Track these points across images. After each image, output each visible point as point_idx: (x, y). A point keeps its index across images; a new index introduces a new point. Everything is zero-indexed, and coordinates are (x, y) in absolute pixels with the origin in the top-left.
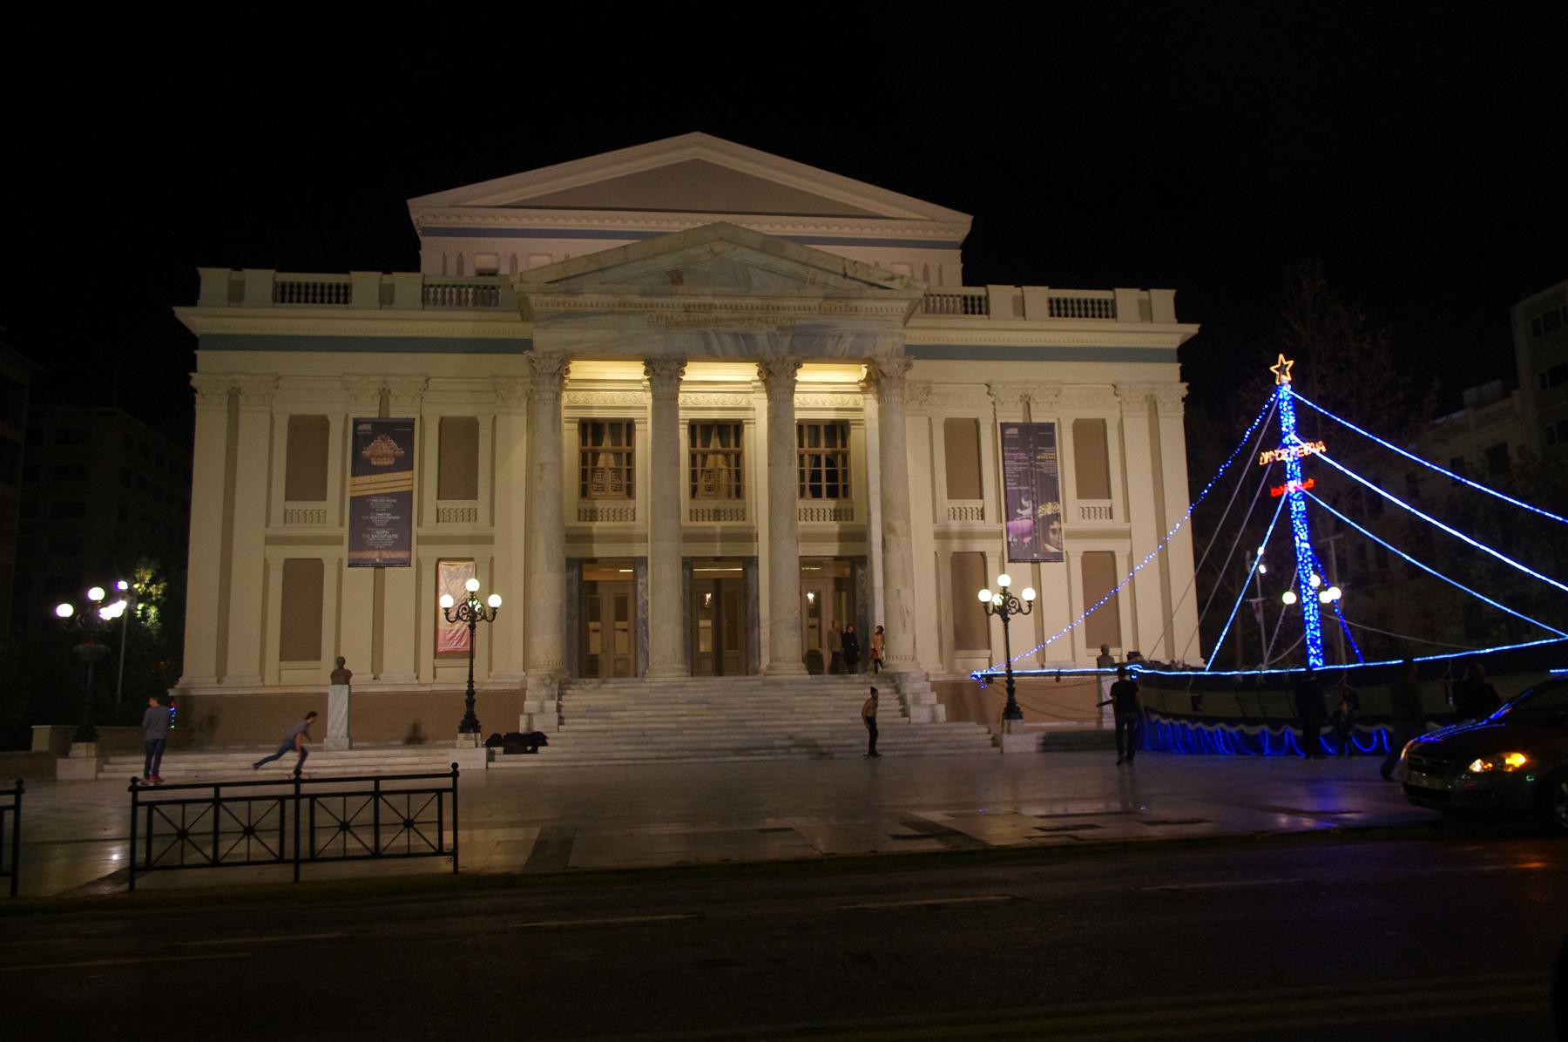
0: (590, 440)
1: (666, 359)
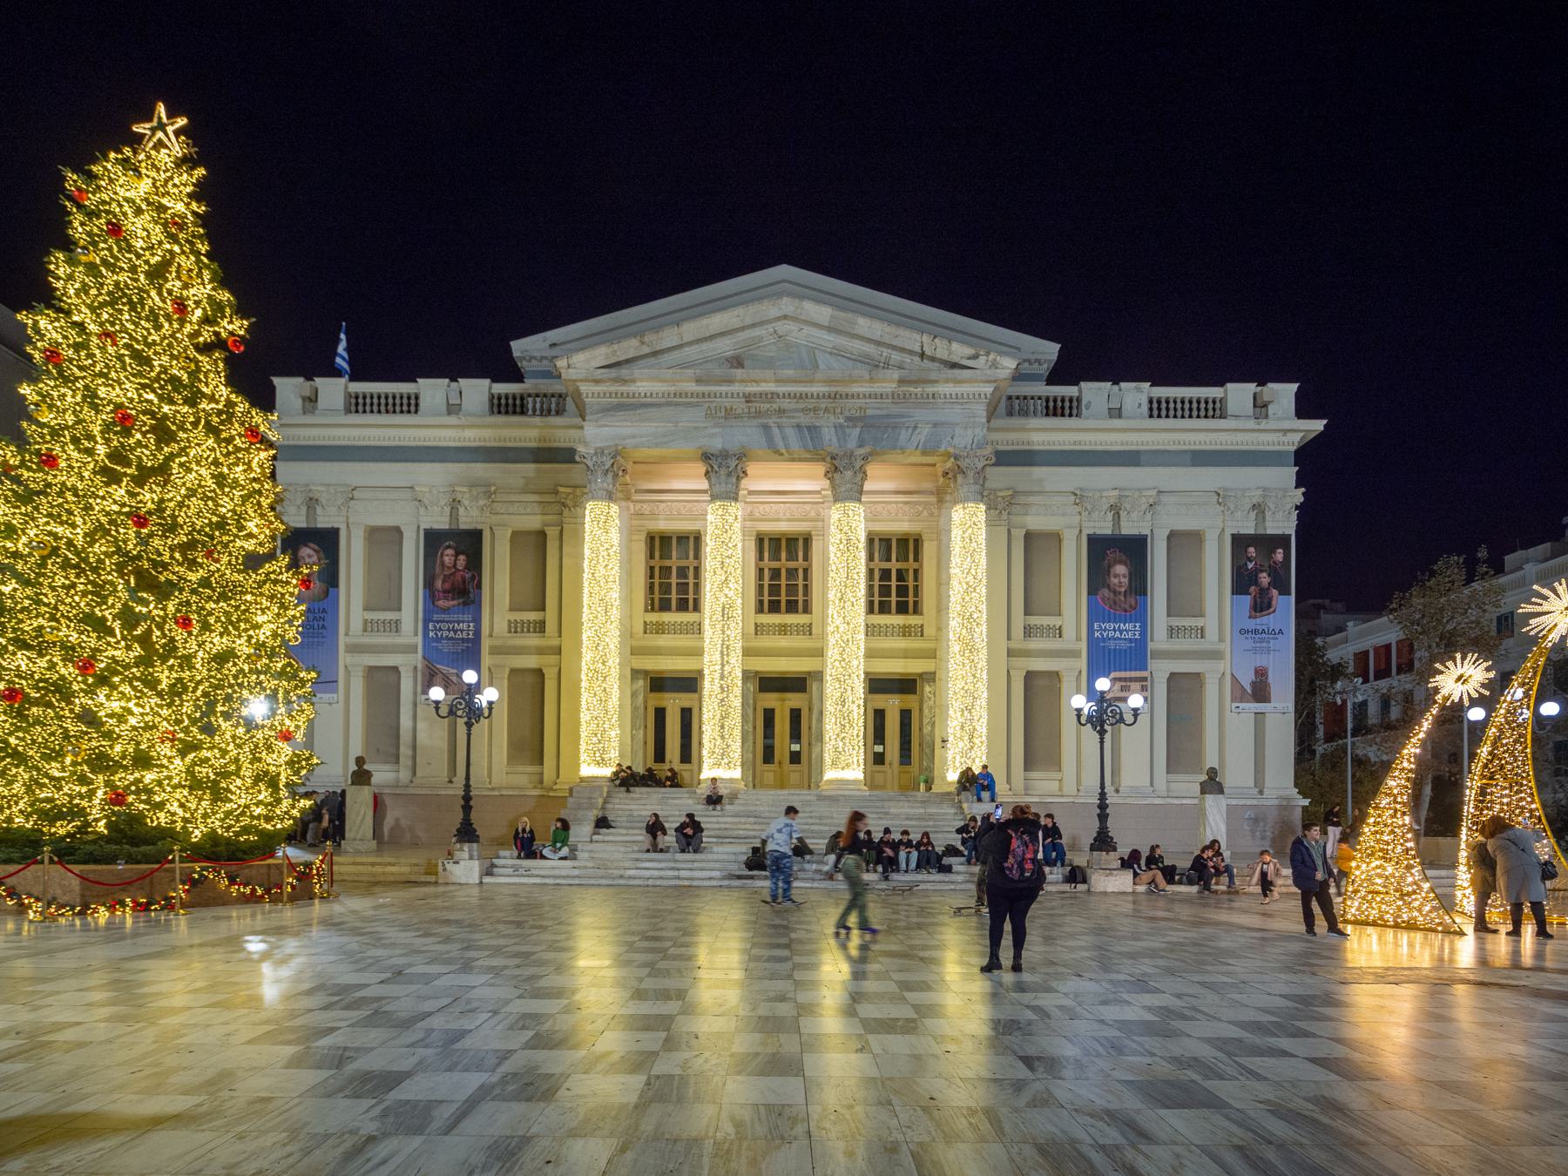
0: (657, 554)
1: (725, 455)
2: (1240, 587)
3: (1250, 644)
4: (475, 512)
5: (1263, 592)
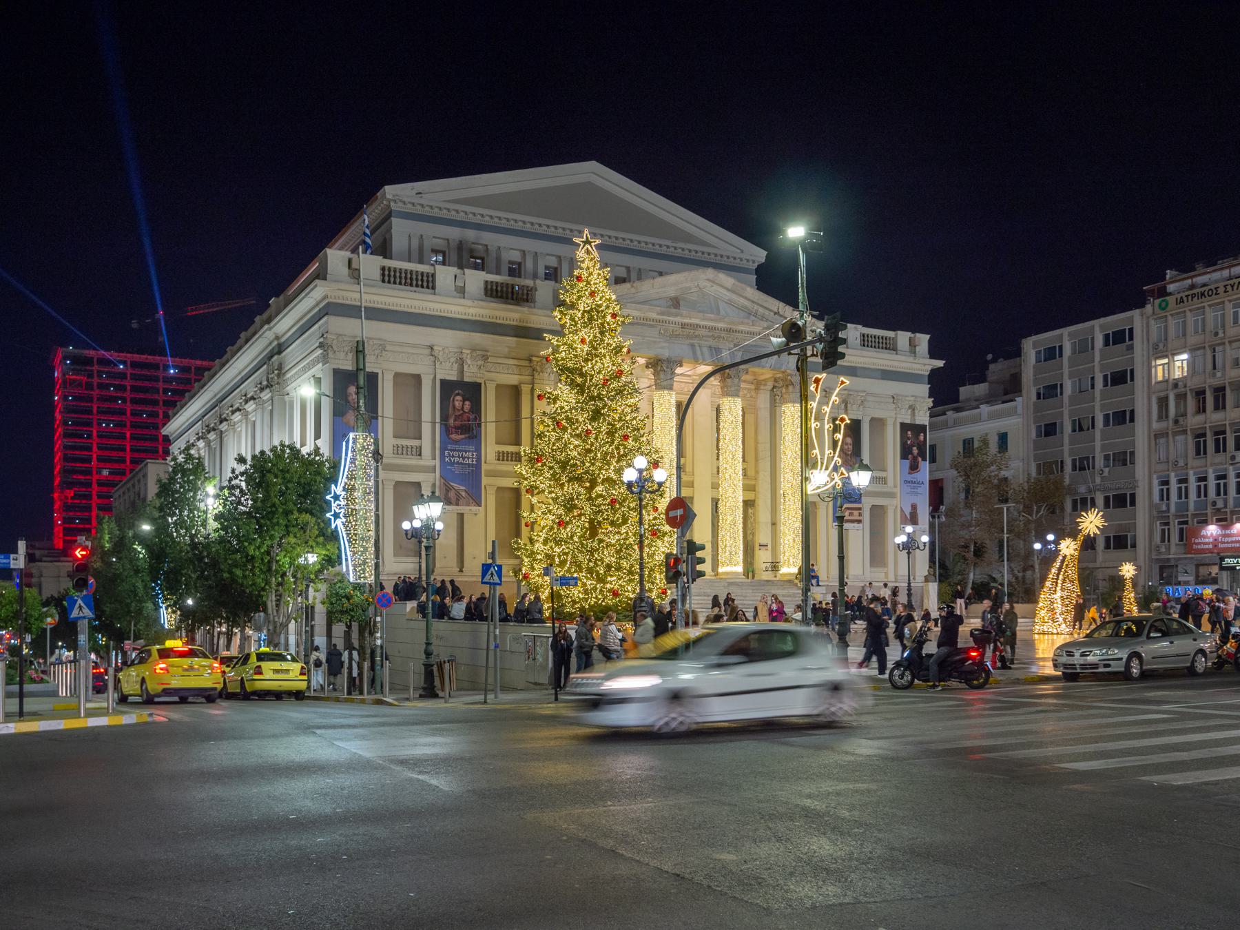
2: (904, 456)
3: (909, 490)
4: (475, 369)
5: (915, 458)
